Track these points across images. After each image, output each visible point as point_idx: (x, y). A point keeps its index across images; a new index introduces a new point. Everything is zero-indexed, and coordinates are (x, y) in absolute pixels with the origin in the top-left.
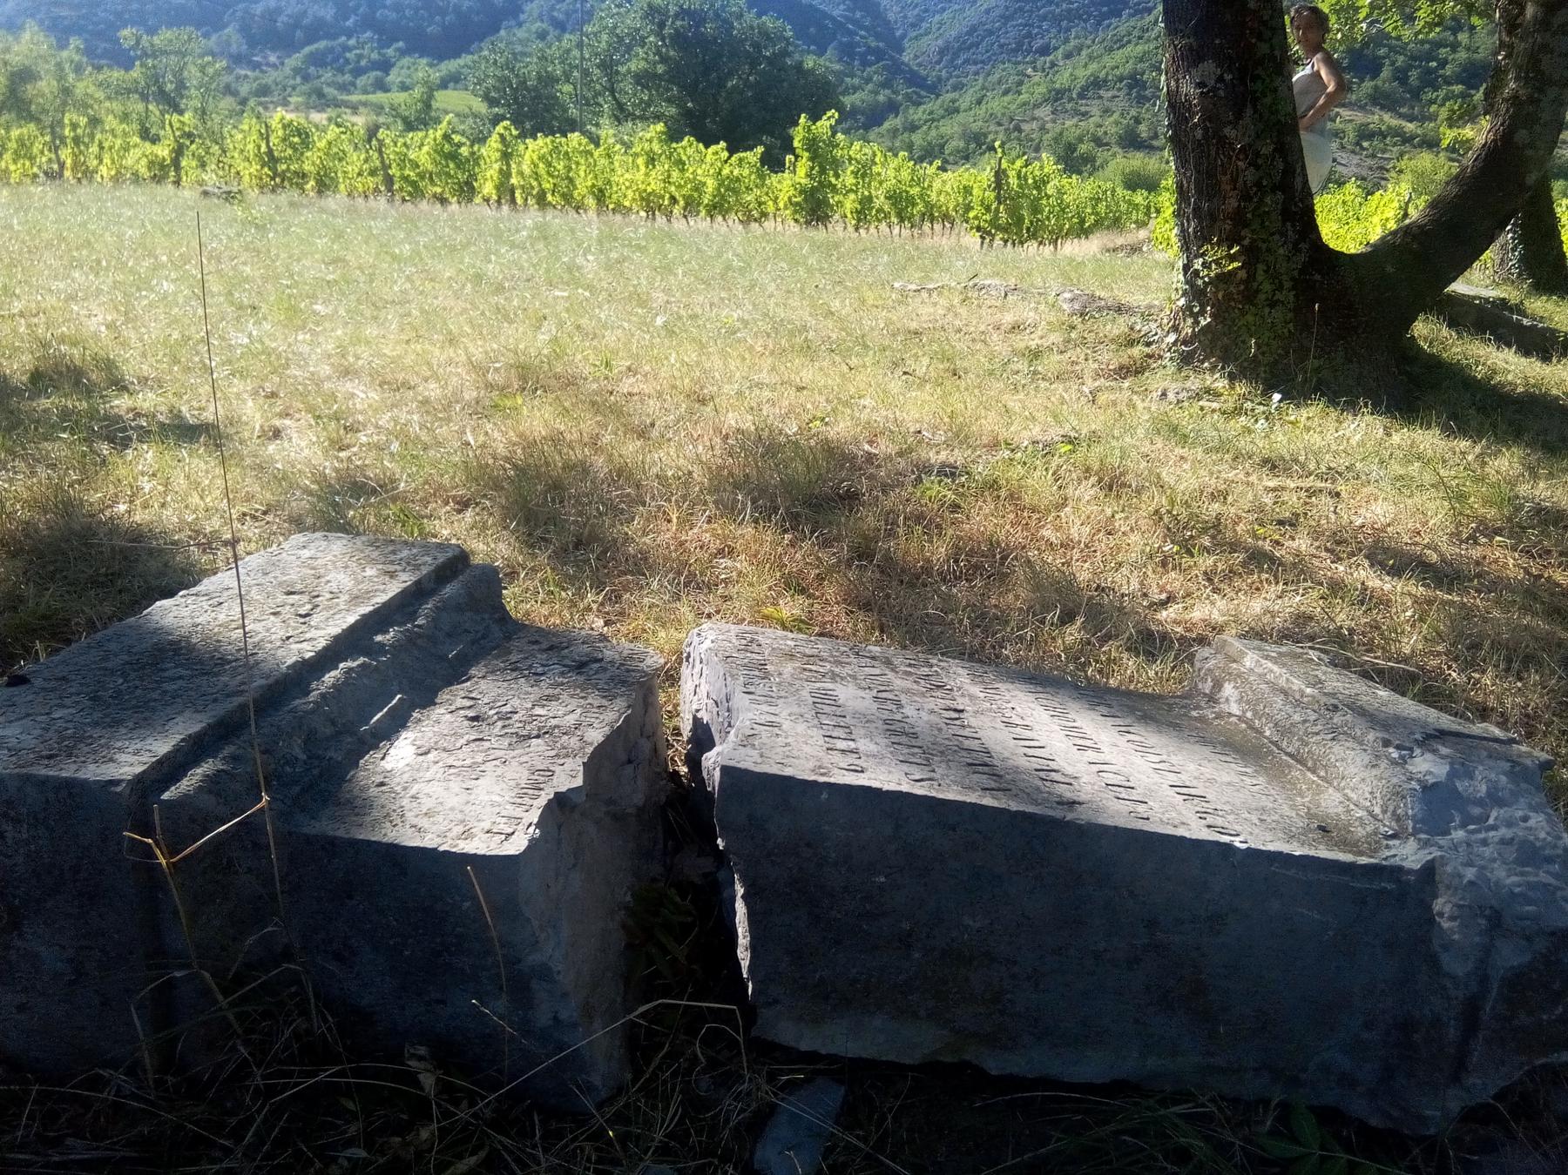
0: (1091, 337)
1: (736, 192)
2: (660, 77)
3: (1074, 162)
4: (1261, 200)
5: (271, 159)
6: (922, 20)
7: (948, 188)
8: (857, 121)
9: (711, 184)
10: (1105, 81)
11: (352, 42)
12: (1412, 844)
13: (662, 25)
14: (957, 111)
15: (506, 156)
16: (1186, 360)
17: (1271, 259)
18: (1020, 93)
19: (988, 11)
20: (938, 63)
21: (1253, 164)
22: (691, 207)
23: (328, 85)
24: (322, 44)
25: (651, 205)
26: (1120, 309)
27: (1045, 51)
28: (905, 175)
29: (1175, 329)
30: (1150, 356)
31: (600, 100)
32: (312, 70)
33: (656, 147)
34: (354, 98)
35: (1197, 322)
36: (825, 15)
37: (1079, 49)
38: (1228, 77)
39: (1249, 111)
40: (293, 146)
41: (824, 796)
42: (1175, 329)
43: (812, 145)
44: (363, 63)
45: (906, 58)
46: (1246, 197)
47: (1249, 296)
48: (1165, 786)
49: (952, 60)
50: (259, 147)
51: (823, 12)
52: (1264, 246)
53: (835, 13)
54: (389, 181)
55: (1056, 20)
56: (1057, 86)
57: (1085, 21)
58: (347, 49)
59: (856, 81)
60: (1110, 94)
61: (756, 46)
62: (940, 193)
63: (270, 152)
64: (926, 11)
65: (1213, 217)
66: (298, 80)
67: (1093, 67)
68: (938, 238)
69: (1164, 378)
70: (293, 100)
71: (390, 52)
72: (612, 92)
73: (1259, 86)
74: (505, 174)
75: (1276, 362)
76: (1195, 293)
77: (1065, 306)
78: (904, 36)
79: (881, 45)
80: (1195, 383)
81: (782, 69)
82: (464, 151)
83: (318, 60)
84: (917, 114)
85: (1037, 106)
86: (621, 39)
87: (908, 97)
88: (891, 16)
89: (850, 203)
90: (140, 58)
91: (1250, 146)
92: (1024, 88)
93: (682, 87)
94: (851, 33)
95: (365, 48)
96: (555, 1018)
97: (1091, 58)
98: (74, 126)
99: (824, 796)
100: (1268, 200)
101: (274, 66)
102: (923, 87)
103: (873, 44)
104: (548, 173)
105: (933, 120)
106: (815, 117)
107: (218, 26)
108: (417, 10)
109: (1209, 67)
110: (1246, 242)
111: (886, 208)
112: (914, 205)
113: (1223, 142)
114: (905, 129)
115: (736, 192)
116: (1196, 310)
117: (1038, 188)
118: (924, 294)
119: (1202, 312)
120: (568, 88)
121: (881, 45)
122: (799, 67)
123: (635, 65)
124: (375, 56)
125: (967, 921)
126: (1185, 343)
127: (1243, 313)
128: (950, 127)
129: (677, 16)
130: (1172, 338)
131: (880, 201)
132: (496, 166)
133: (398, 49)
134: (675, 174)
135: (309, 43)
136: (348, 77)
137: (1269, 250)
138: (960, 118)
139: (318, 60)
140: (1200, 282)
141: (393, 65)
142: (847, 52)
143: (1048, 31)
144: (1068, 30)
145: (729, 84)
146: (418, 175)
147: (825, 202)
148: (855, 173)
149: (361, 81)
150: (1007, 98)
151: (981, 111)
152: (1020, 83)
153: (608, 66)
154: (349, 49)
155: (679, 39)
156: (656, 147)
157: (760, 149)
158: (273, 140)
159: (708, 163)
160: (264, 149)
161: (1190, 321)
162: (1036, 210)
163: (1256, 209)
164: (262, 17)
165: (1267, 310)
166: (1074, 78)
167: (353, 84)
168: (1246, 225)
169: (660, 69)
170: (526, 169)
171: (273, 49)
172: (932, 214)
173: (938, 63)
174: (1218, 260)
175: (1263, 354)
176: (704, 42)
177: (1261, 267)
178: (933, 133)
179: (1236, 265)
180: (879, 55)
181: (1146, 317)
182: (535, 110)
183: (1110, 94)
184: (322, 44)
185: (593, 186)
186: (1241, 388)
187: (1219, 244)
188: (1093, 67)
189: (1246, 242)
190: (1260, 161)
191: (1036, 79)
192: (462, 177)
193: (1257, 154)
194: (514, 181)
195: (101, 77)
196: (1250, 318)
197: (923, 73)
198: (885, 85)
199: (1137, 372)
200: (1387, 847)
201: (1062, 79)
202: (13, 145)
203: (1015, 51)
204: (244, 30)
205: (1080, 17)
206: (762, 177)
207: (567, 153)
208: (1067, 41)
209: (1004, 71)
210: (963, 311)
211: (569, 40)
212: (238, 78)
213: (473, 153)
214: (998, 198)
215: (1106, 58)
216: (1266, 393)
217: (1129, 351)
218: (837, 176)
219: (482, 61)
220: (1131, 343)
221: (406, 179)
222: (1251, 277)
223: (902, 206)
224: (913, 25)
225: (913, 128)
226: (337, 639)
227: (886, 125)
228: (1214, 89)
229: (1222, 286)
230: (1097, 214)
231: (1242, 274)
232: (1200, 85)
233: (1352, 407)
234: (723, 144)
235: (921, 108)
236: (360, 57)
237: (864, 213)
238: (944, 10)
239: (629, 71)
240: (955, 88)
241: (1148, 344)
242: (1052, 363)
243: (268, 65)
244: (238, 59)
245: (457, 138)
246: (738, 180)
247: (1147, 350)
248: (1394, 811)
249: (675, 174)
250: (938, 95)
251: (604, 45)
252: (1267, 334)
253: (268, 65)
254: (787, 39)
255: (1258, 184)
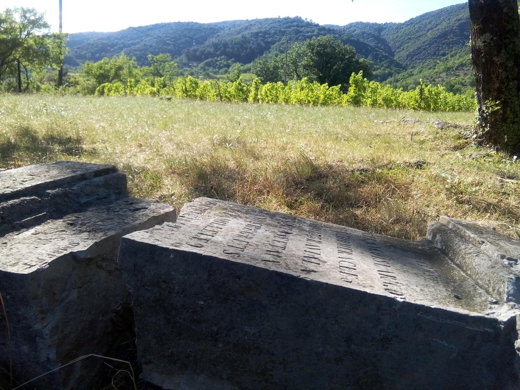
0: (444, 137)
1: (331, 99)
2: (311, 66)
3: (452, 89)
4: (508, 83)
5: (186, 91)
6: (401, 46)
7: (405, 97)
8: (378, 79)
9: (322, 97)
10: (465, 64)
11: (218, 59)
12: (506, 307)
13: (313, 49)
14: (413, 75)
15: (257, 89)
16: (480, 144)
17: (513, 106)
19: (424, 42)
20: (406, 60)
21: (505, 70)
22: (315, 103)
23: (211, 72)
24: (209, 60)
25: (300, 102)
26: (456, 127)
27: (444, 55)
28: (389, 92)
29: (476, 133)
30: (466, 143)
31: (292, 74)
32: (206, 67)
33: (304, 85)
34: (218, 76)
35: (484, 130)
36: (368, 45)
37: (456, 54)
38: (495, 38)
39: (503, 51)
40: (193, 87)
41: (172, 256)
42: (476, 133)
43: (356, 82)
44: (222, 65)
45: (395, 58)
46: (502, 83)
47: (504, 119)
48: (376, 270)
49: (411, 59)
50: (183, 87)
52: (510, 101)
53: (372, 45)
54: (221, 98)
55: (448, 44)
56: (448, 66)
57: (458, 44)
58: (217, 61)
59: (378, 66)
60: (467, 68)
61: (343, 55)
62: (402, 99)
63: (186, 89)
64: (403, 43)
65: (490, 91)
66: (202, 71)
67: (461, 60)
68: (400, 114)
69: (472, 151)
70: (200, 77)
71: (230, 62)
72: (296, 71)
73: (507, 41)
74: (256, 95)
75: (515, 145)
76: (483, 119)
77: (436, 126)
78: (395, 51)
79: (387, 54)
80: (483, 152)
81: (352, 62)
82: (245, 88)
83: (208, 65)
84: (399, 76)
85: (440, 73)
86: (299, 54)
87: (396, 71)
88: (390, 45)
89: (369, 101)
90: (153, 63)
91: (504, 63)
92: (436, 67)
93: (319, 69)
94: (377, 51)
95: (222, 60)
96: (48, 358)
97: (460, 56)
98: (131, 82)
99: (172, 256)
100: (511, 83)
101: (195, 67)
102: (401, 67)
103: (384, 54)
104: (270, 95)
105: (404, 78)
106: (357, 73)
107: (180, 55)
108: (238, 48)
109: (487, 36)
110: (503, 99)
111: (382, 103)
112: (393, 102)
113: (493, 62)
114: (394, 81)
115: (331, 99)
116: (484, 125)
117: (436, 96)
118: (385, 124)
119: (486, 126)
120: (282, 71)
121: (387, 54)
122: (357, 62)
123: (303, 63)
124: (225, 63)
125: (247, 329)
126: (480, 138)
127: (502, 126)
128: (410, 80)
129: (318, 46)
130: (475, 136)
131: (380, 101)
132: (254, 92)
133: (232, 61)
134: (310, 93)
135: (205, 59)
136: (217, 70)
137: (511, 102)
138: (414, 77)
139: (208, 65)
140: (485, 115)
141: (230, 66)
142: (375, 57)
143: (445, 48)
144: (452, 47)
145: (334, 68)
146: (230, 96)
147: (360, 100)
148: (371, 92)
149: (221, 71)
150: (430, 71)
152: (435, 66)
153: (295, 63)
154: (218, 61)
155: (318, 53)
156: (304, 85)
157: (340, 85)
158: (187, 85)
159: (321, 90)
160: (184, 88)
161: (481, 129)
162: (436, 103)
163: (506, 87)
164: (193, 51)
165: (511, 125)
166: (454, 63)
167: (218, 72)
168: (502, 93)
169: (311, 63)
170: (263, 93)
171: (195, 61)
172: (399, 106)
173: (406, 60)
174: (492, 106)
175: (510, 141)
176: (327, 54)
177: (508, 109)
178: (404, 82)
179: (498, 108)
180: (386, 57)
181: (466, 129)
182: (269, 76)
183: (467, 68)
184: (209, 60)
185: (285, 98)
186: (502, 154)
187: (492, 100)
188: (461, 60)
189: (503, 99)
190: (508, 69)
191: (441, 64)
192: (244, 96)
193: (507, 66)
194: (259, 97)
195: (142, 69)
196: (505, 128)
197: (401, 63)
198: (388, 67)
199: (461, 148)
200: (491, 308)
201: (450, 64)
202: (114, 88)
203: (433, 55)
204: (187, 56)
205: (456, 43)
206: (340, 94)
207: (276, 88)
208: (452, 51)
209: (430, 62)
210: (398, 129)
211: (283, 55)
212: (185, 70)
213: (248, 89)
214: (421, 98)
215: (466, 57)
216: (511, 156)
217: (458, 141)
218: (364, 92)
219: (257, 64)
220: (459, 138)
221: (226, 97)
222: (505, 113)
223: (388, 102)
224: (398, 48)
225: (397, 81)
226: (27, 189)
227: (388, 80)
228: (489, 43)
229: (494, 116)
230: (460, 106)
231: (501, 112)
232: (484, 42)
234: (327, 84)
235: (400, 75)
236: (221, 63)
237: (374, 103)
238: (408, 42)
239: (302, 65)
240: (412, 68)
241: (466, 139)
242: (429, 145)
243: (193, 66)
244: (185, 65)
245: (243, 84)
246: (331, 95)
247: (465, 141)
248: (498, 290)
249: (310, 93)
250: (406, 70)
251: (294, 57)
252: (512, 134)
253: (193, 66)
254: (353, 53)
255: (507, 77)
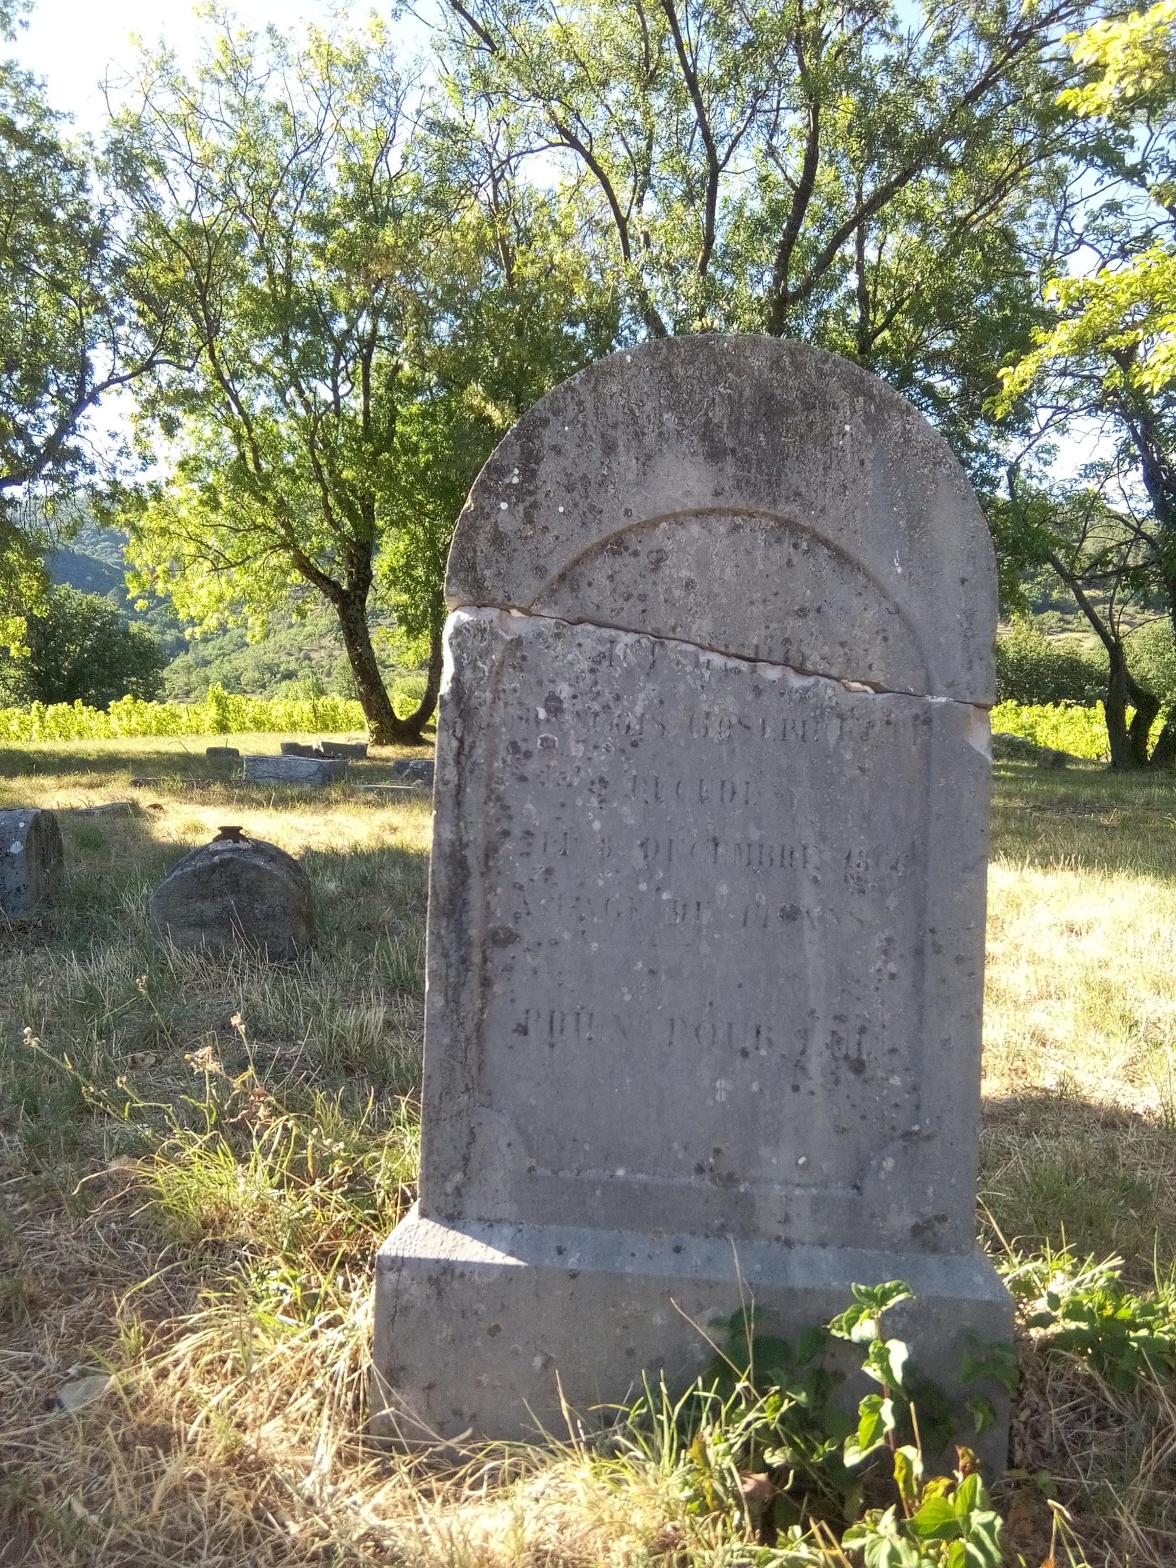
18: (304, 625)
51: (96, 561)
105: (224, 655)
138: (248, 651)
151: (270, 644)
225: (206, 663)
233: (1110, 862)
